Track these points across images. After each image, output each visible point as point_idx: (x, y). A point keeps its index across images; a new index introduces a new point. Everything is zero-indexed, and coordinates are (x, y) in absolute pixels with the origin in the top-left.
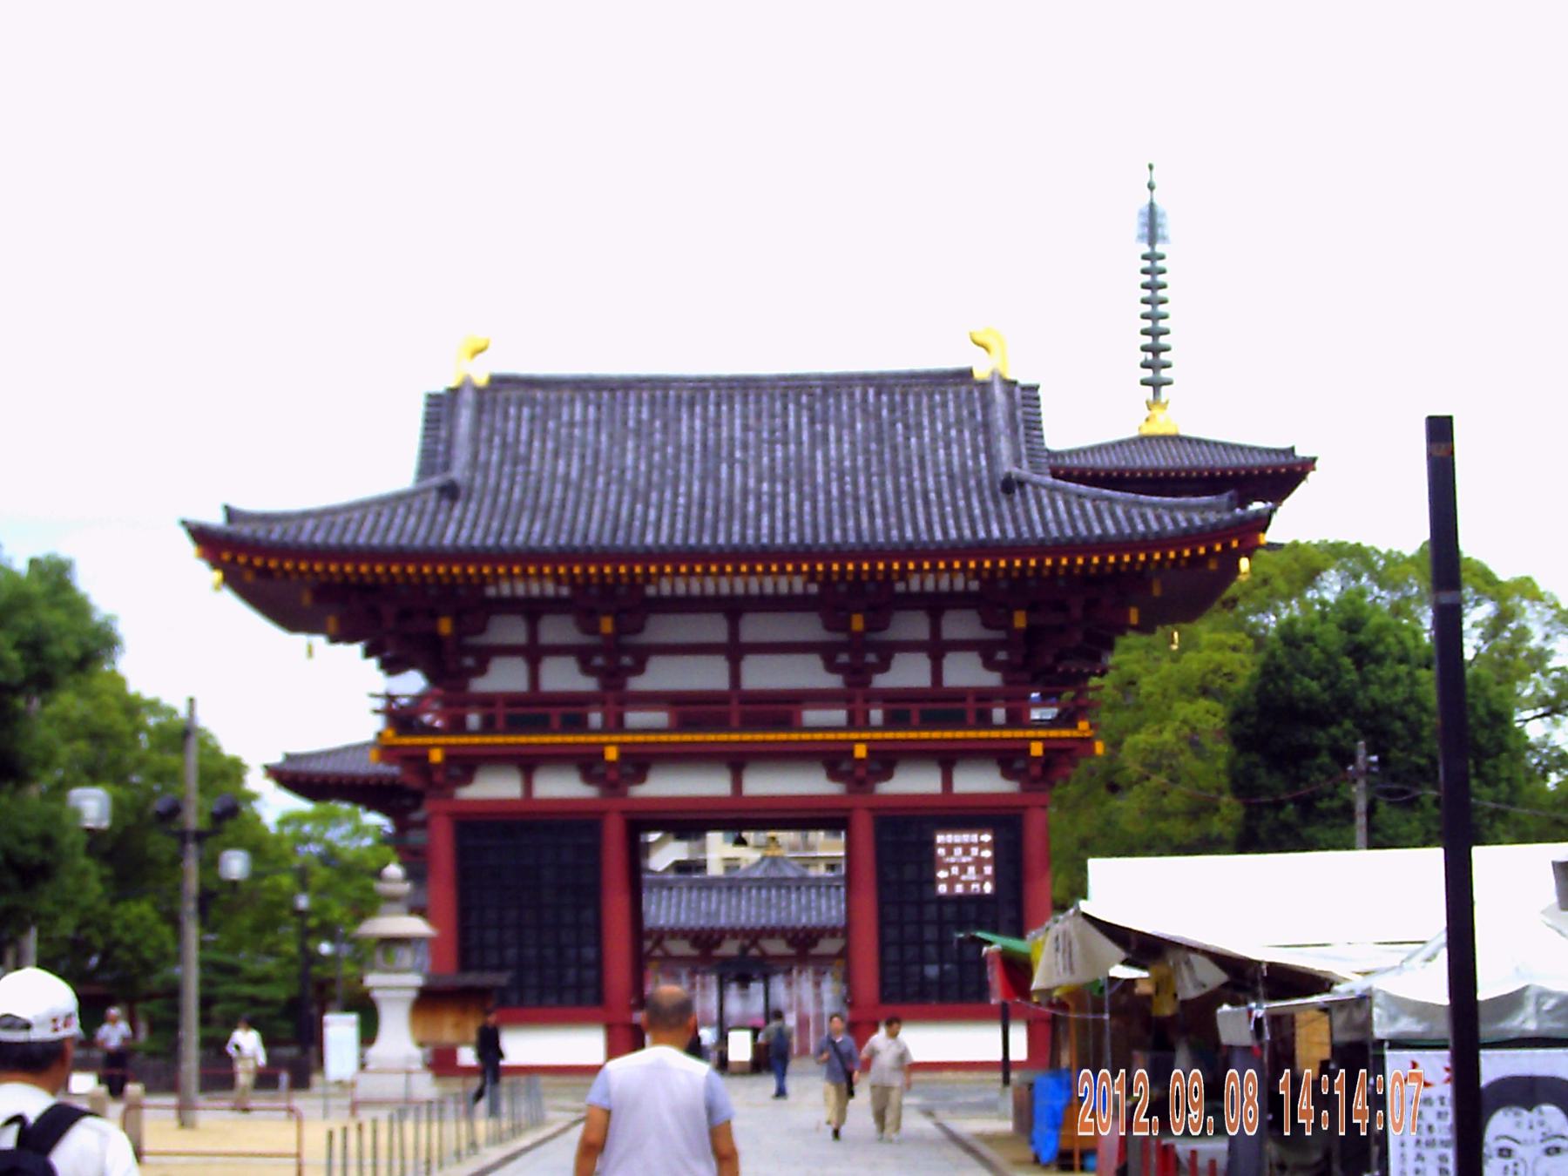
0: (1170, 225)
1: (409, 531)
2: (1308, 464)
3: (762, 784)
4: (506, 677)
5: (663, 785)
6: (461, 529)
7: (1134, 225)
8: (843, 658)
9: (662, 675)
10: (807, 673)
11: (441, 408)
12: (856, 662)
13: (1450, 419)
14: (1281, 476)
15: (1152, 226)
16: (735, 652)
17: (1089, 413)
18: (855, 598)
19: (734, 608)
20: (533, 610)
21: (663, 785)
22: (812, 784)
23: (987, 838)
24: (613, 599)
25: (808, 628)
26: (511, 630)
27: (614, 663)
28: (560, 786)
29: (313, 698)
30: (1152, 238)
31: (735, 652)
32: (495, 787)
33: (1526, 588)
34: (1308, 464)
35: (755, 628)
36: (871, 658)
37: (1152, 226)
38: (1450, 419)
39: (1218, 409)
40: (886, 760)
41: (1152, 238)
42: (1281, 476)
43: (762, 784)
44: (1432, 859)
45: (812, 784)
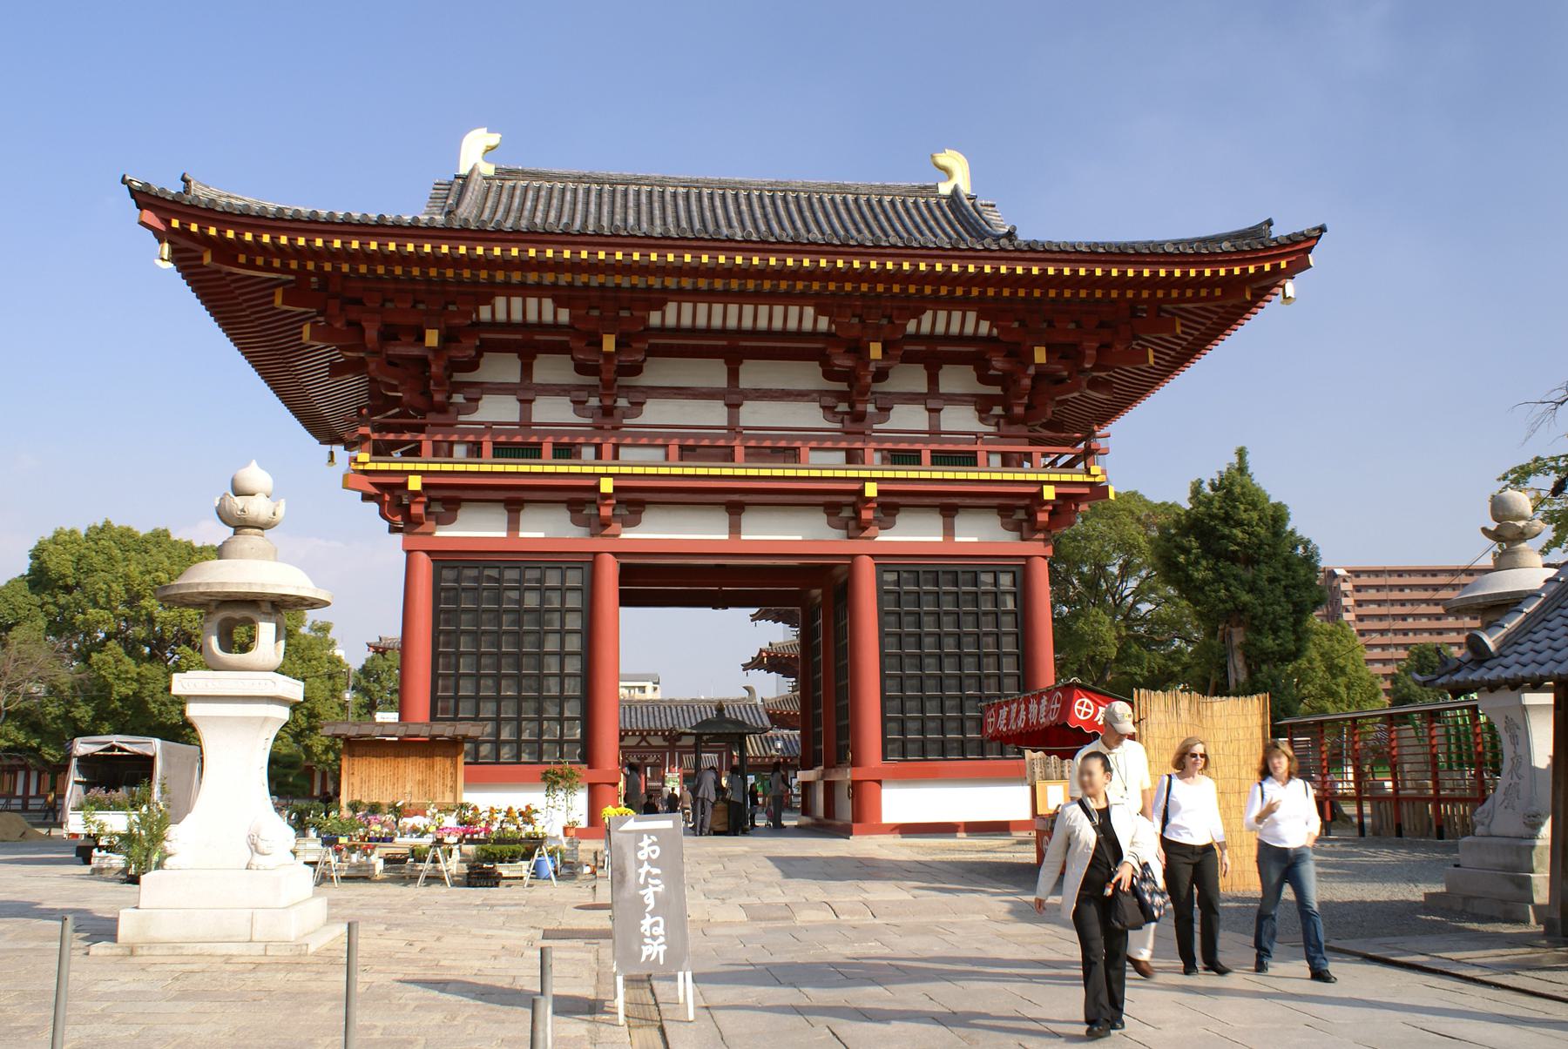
5: (658, 532)
9: (657, 413)
10: (808, 416)
14: (1269, 223)
16: (733, 398)
25: (807, 376)
28: (543, 529)
31: (733, 398)
35: (753, 375)
40: (892, 505)
42: (1269, 223)
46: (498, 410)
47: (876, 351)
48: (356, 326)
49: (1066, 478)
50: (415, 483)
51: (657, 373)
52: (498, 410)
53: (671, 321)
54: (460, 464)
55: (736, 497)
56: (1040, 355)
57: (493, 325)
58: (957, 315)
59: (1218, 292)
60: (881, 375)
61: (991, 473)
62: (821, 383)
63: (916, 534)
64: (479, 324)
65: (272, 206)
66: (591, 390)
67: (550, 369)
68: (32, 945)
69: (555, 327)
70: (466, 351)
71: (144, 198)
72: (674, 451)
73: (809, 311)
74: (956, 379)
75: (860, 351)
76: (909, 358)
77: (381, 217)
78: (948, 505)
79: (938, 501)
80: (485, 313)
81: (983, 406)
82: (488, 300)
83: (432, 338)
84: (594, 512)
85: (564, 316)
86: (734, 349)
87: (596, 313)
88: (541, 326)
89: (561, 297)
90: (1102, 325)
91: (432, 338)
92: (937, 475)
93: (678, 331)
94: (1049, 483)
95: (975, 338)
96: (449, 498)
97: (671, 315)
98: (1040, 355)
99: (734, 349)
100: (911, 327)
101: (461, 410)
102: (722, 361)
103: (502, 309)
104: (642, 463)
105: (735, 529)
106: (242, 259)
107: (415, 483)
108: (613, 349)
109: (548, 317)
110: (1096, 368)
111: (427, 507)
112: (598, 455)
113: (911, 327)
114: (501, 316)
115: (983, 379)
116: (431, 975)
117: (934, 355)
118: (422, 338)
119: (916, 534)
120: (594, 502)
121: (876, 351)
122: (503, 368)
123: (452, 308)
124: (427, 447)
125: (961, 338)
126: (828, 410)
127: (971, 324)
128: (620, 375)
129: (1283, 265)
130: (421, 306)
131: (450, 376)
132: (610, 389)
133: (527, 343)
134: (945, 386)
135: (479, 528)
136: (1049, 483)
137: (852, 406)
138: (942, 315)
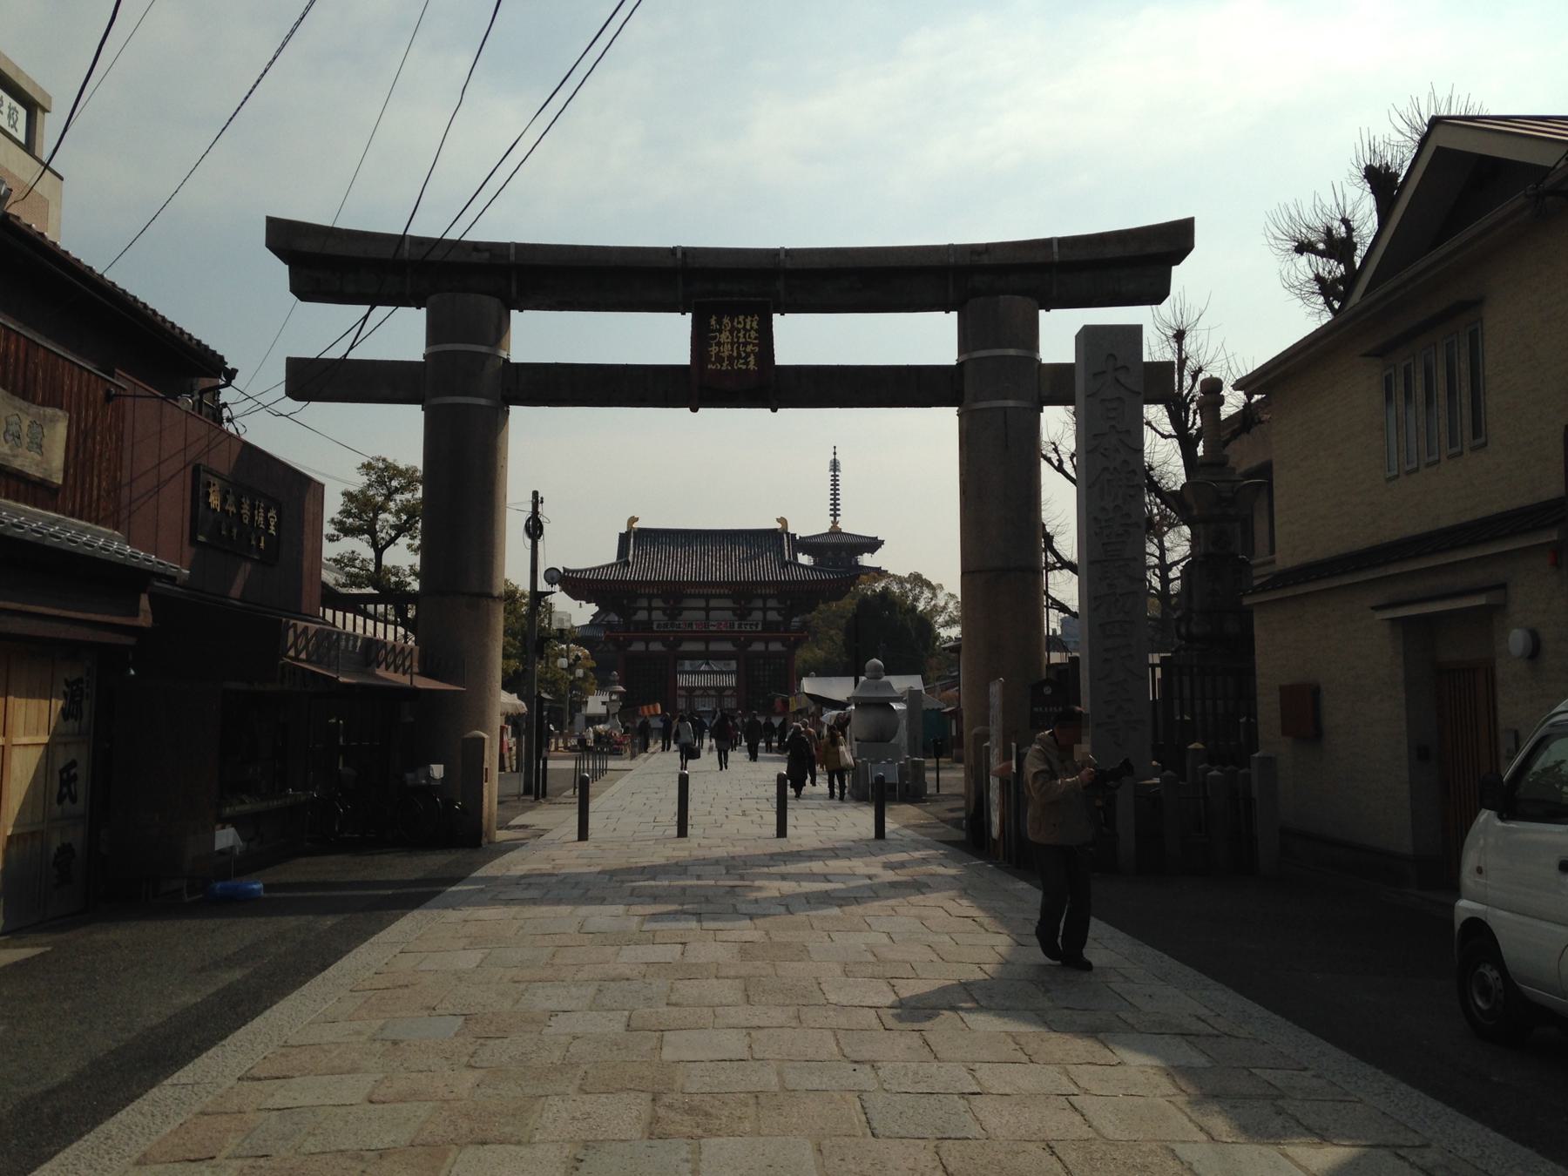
0: (842, 466)
1: (613, 575)
2: (882, 542)
3: (714, 647)
4: (642, 615)
5: (688, 647)
6: (631, 574)
7: (828, 466)
11: (624, 539)
12: (743, 614)
13: (289, 360)
14: (873, 545)
15: (835, 466)
17: (809, 522)
18: (742, 594)
19: (707, 598)
20: (765, 598)
21: (688, 647)
22: (728, 647)
23: (752, 366)
24: (673, 593)
25: (728, 603)
26: (759, 603)
27: (673, 613)
29: (577, 613)
30: (835, 516)
32: (638, 647)
33: (941, 587)
34: (882, 542)
35: (713, 603)
37: (835, 466)
38: (289, 360)
39: (853, 524)
41: (835, 516)
42: (873, 545)
43: (714, 647)
44: (852, 679)
45: (728, 647)
74: (772, 603)
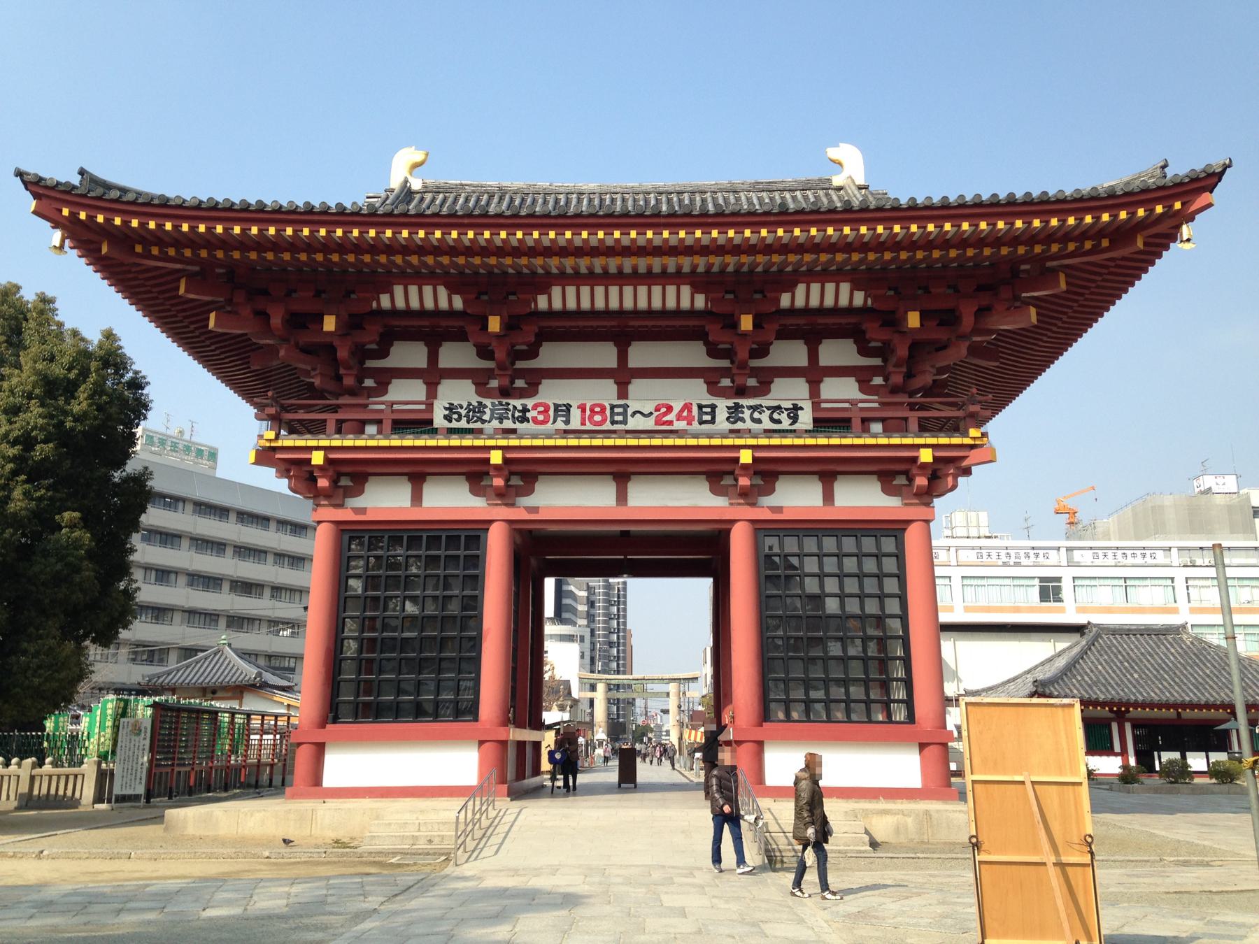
8: (878, 381)
9: (551, 393)
16: (623, 377)
25: (693, 354)
28: (449, 500)
36: (752, 382)
46: (407, 393)
47: (746, 323)
48: (263, 316)
49: (944, 441)
50: (318, 458)
51: (553, 355)
52: (407, 393)
53: (800, 302)
54: (372, 439)
55: (359, 469)
56: (914, 320)
57: (550, 314)
58: (830, 287)
59: (1105, 243)
60: (762, 351)
61: (877, 437)
62: (705, 361)
63: (797, 498)
64: (380, 312)
65: (1085, 186)
66: (725, 372)
67: (454, 355)
68: (1141, 880)
69: (451, 313)
70: (369, 339)
71: (35, 185)
72: (387, 425)
73: (845, 288)
74: (836, 352)
75: (893, 321)
76: (786, 334)
77: (913, 199)
78: (828, 471)
79: (406, 470)
80: (542, 303)
81: (862, 376)
82: (546, 290)
83: (330, 324)
84: (732, 482)
85: (458, 303)
86: (622, 329)
87: (730, 296)
88: (437, 313)
89: (699, 282)
90: (980, 288)
91: (330, 324)
92: (396, 442)
93: (565, 314)
94: (318, 448)
95: (850, 310)
96: (351, 474)
97: (559, 299)
98: (914, 320)
99: (622, 329)
100: (785, 300)
101: (371, 392)
102: (802, 342)
103: (402, 297)
104: (537, 436)
105: (417, 498)
106: (139, 249)
107: (318, 458)
108: (750, 327)
109: (443, 304)
110: (976, 331)
111: (507, 480)
112: (380, 432)
113: (785, 300)
114: (557, 305)
115: (863, 351)
116: (882, 891)
117: (813, 327)
118: (735, 325)
119: (797, 498)
120: (732, 473)
121: (746, 323)
122: (410, 354)
123: (512, 298)
124: (331, 426)
125: (836, 311)
126: (865, 386)
127: (843, 295)
128: (751, 357)
129: (1178, 205)
130: (485, 298)
131: (513, 364)
132: (510, 374)
133: (433, 330)
134: (445, 362)
135: (386, 501)
136: (318, 448)
137: (886, 380)
138: (815, 288)
